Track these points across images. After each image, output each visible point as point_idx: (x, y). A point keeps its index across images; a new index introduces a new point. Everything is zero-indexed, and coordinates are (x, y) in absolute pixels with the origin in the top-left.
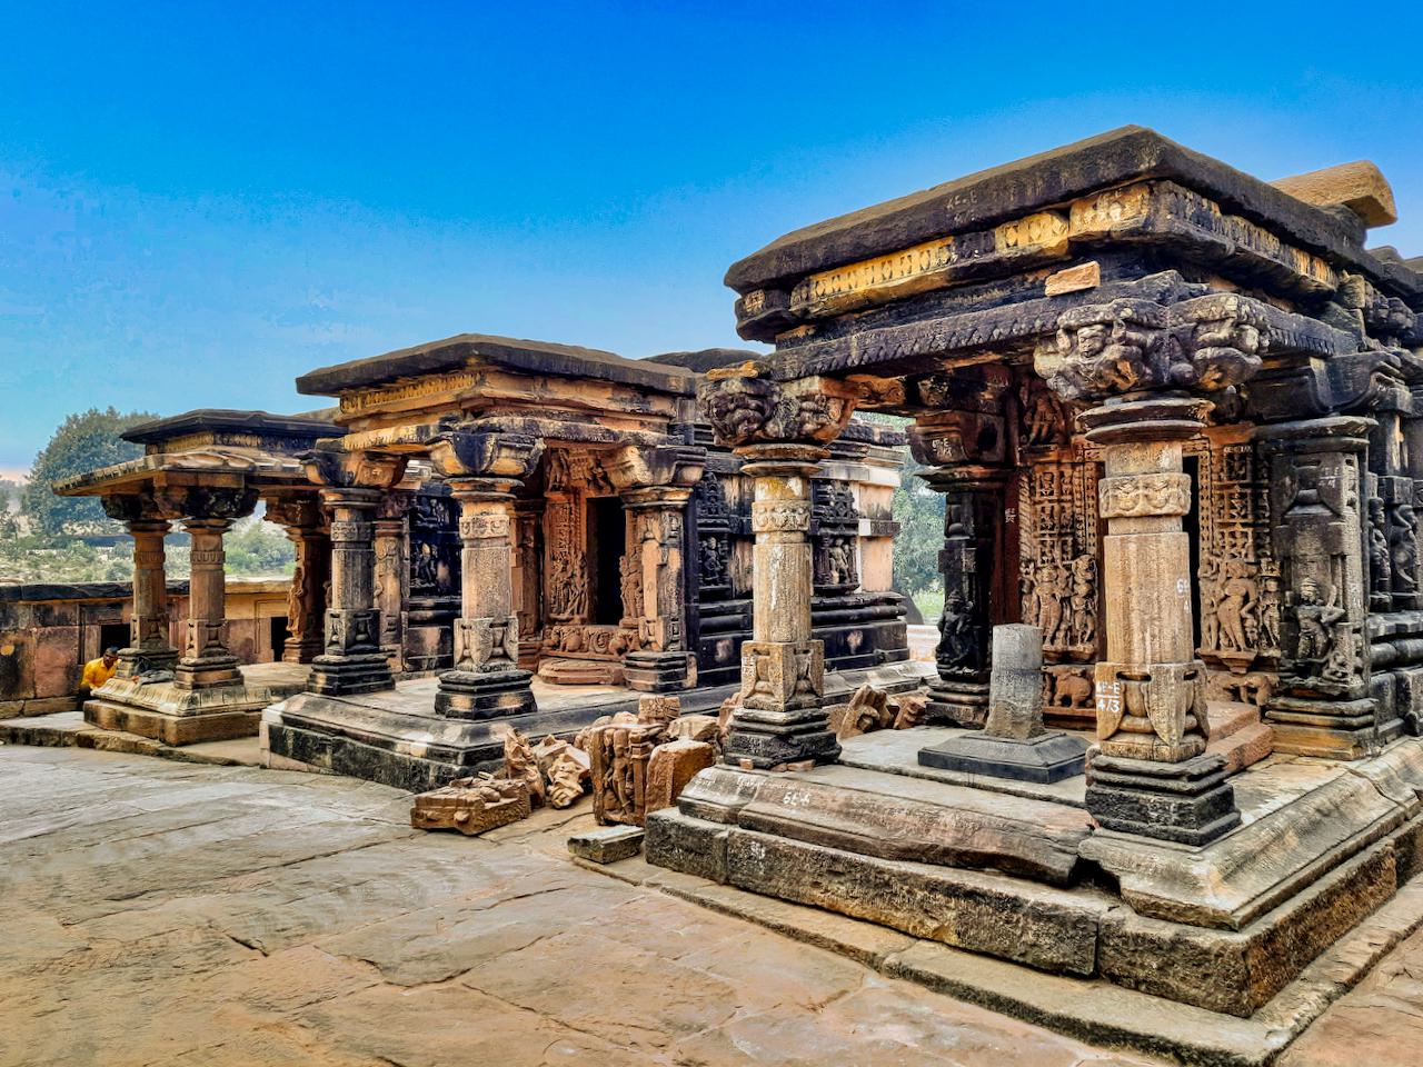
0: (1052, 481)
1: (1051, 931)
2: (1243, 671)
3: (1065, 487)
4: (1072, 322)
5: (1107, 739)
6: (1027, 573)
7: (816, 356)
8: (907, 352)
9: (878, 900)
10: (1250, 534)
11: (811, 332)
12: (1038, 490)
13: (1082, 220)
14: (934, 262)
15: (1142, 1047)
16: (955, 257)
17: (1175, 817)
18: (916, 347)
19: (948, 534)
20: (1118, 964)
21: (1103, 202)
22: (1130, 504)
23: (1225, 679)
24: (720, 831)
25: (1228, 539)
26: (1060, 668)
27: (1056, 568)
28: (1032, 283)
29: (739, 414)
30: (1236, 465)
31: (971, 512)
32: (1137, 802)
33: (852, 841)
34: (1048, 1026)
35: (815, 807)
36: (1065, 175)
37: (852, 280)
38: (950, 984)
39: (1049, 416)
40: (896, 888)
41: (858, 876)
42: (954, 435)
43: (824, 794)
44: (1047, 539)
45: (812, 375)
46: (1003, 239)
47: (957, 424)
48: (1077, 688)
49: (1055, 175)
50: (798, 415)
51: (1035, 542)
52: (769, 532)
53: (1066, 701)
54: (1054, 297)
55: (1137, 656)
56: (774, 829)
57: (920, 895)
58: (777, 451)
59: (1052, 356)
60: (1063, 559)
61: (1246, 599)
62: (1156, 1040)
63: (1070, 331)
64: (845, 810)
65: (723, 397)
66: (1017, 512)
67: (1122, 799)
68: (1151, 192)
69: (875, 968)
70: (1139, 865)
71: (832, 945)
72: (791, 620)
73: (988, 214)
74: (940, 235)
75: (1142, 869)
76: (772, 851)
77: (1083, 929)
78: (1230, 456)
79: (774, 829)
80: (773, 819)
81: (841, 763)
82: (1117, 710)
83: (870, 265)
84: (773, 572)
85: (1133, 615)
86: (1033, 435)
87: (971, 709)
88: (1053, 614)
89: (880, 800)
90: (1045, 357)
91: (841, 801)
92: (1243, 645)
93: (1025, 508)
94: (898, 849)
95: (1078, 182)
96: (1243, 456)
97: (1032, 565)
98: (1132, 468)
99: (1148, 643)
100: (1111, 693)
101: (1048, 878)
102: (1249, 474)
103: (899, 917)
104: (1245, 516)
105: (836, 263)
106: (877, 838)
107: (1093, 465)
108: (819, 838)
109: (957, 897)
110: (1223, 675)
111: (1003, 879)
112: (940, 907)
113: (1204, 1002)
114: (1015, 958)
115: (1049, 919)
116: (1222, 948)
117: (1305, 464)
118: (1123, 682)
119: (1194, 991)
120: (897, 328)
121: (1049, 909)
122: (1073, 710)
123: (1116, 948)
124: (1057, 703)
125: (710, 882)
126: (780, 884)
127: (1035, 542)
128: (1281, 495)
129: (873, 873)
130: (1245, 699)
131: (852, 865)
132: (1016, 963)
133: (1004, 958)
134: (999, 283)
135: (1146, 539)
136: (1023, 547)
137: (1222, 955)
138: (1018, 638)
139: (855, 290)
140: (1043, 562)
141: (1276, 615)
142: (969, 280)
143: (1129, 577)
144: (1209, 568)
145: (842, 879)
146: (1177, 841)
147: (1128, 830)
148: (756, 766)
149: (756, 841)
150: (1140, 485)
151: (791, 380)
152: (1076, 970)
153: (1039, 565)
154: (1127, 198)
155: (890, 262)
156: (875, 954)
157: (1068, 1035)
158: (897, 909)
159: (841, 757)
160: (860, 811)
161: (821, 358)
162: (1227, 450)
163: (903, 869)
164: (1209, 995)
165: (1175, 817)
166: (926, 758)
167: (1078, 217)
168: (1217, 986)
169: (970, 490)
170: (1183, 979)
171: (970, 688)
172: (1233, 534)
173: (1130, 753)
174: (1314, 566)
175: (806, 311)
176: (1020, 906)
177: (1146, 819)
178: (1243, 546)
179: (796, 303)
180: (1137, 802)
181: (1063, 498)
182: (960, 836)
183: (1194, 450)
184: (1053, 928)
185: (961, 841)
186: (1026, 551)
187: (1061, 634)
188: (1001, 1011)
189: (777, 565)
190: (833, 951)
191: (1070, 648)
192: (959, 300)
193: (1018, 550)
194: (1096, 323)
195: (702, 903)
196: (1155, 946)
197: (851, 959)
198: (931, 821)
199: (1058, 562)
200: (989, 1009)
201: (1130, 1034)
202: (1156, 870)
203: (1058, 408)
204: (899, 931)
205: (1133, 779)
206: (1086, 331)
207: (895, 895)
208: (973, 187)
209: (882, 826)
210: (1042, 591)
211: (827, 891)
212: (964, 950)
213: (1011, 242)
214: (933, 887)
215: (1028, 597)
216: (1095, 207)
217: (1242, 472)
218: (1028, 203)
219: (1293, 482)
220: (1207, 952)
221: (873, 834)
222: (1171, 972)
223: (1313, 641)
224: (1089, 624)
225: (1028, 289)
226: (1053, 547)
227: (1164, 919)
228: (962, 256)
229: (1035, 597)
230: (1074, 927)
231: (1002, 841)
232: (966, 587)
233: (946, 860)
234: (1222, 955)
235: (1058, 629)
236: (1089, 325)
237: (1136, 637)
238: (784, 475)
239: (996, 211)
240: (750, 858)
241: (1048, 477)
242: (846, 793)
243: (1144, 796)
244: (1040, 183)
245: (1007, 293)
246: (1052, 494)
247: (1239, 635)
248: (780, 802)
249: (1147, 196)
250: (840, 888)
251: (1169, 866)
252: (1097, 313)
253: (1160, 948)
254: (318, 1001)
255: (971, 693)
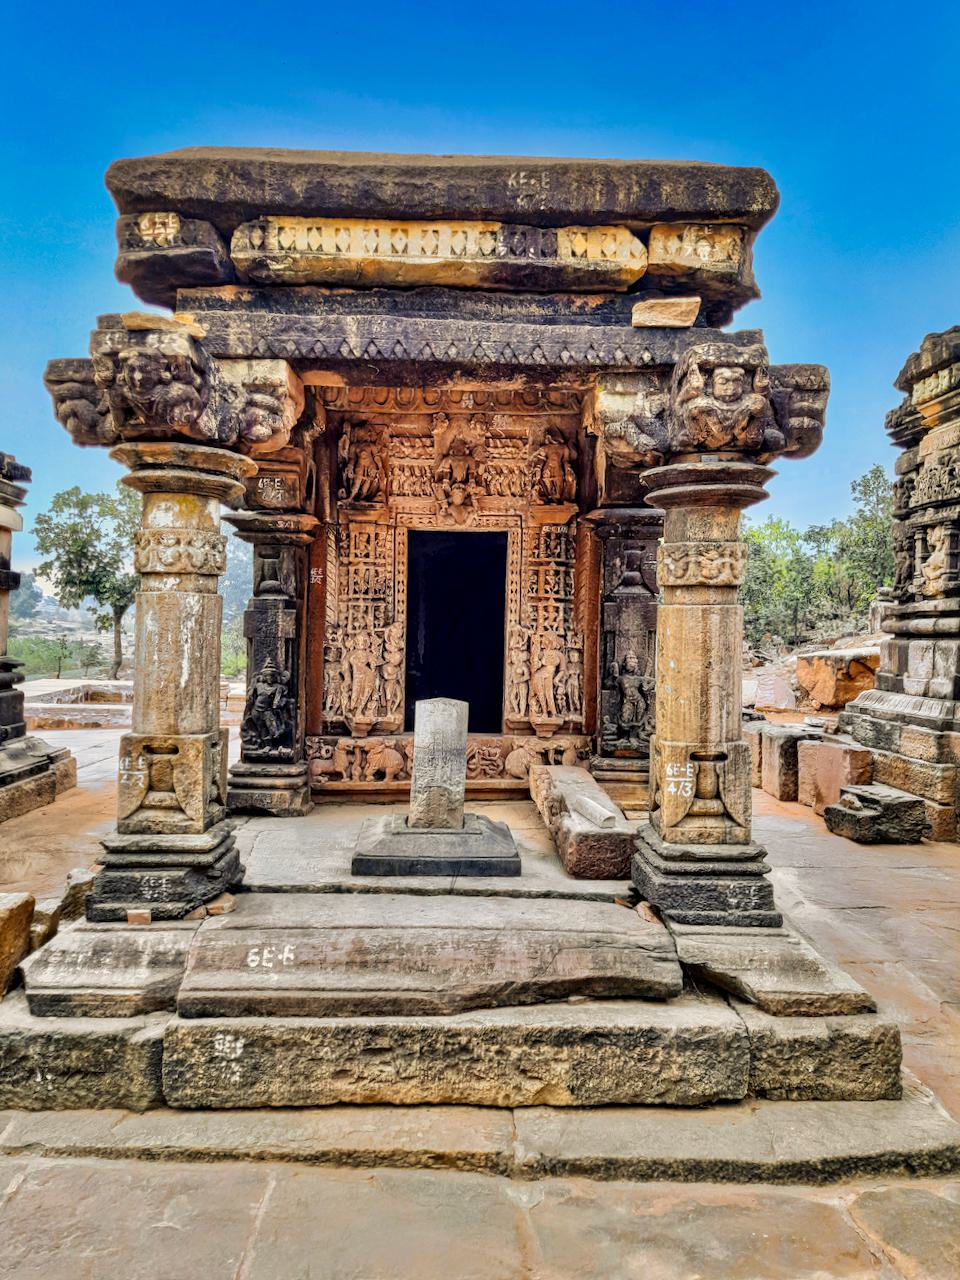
0: (368, 541)
1: (701, 1059)
2: (550, 735)
4: (712, 359)
5: (675, 826)
6: (333, 640)
7: (284, 331)
8: (439, 355)
9: (450, 1075)
10: (561, 609)
11: (246, 297)
12: (353, 550)
13: (666, 249)
14: (472, 248)
15: (874, 1169)
16: (502, 250)
17: (755, 900)
18: (453, 352)
19: (257, 593)
20: (771, 1077)
21: (690, 235)
22: (715, 572)
23: (535, 744)
24: (136, 1030)
25: (542, 613)
26: (373, 740)
28: (581, 307)
29: (177, 389)
30: (553, 544)
32: (715, 890)
33: (395, 1002)
34: (768, 1179)
35: (306, 964)
36: (666, 189)
37: (343, 239)
38: (627, 1164)
39: (373, 472)
40: (478, 1051)
41: (417, 1047)
42: (293, 476)
43: (313, 941)
45: (274, 357)
46: (568, 245)
48: (392, 761)
49: (654, 186)
50: (244, 411)
52: (179, 574)
53: (380, 775)
54: (640, 328)
55: (713, 735)
56: (250, 1008)
57: (515, 1052)
58: (207, 457)
59: (617, 397)
61: (558, 669)
62: (887, 1157)
63: (707, 370)
64: (358, 959)
65: (154, 358)
66: (324, 573)
67: (699, 889)
68: (742, 240)
69: (502, 1173)
70: (751, 960)
71: (424, 1158)
72: (207, 702)
73: (564, 207)
74: (486, 216)
75: (755, 964)
76: (257, 1043)
77: (737, 1049)
78: (548, 535)
79: (250, 1008)
80: (242, 994)
81: (248, 889)
82: (689, 793)
83: (372, 226)
84: (185, 634)
85: (712, 691)
86: (355, 491)
87: (287, 794)
89: (407, 937)
90: (610, 397)
91: (349, 947)
92: (554, 712)
93: (332, 568)
94: (464, 998)
95: (682, 202)
96: (558, 536)
98: (716, 534)
99: (724, 720)
100: (684, 774)
101: (651, 994)
102: (563, 554)
103: (483, 1089)
104: (557, 592)
105: (320, 208)
106: (431, 991)
107: (405, 530)
108: (334, 1008)
109: (572, 1044)
110: (534, 739)
111: (594, 1006)
112: (546, 1062)
113: (862, 1094)
114: (649, 1100)
115: (698, 1045)
116: (883, 1034)
117: (632, 548)
118: (696, 763)
119: (851, 1086)
120: (422, 323)
121: (697, 1034)
122: (388, 783)
123: (771, 1062)
125: (119, 1113)
126: (273, 1088)
127: (343, 606)
128: (611, 574)
129: (442, 1039)
130: (552, 762)
131: (404, 1035)
132: (652, 1106)
133: (635, 1104)
134: (537, 297)
135: (727, 610)
136: (329, 612)
137: (883, 1042)
138: (455, 715)
139: (344, 255)
140: (354, 628)
141: (576, 683)
142: (510, 284)
143: (708, 651)
145: (388, 1057)
146: (760, 926)
147: (708, 921)
148: (157, 917)
149: (226, 1032)
150: (728, 552)
151: (236, 358)
152: (730, 1096)
153: (350, 630)
154: (717, 238)
155: (405, 231)
156: (498, 1154)
157: (793, 1183)
158: (479, 1078)
159: (246, 881)
160: (383, 957)
161: (294, 335)
162: (546, 529)
163: (489, 1025)
164: (867, 1084)
165: (755, 900)
166: (362, 866)
167: (661, 244)
168: (876, 1075)
169: (292, 543)
170: (840, 1076)
171: (286, 769)
172: (546, 609)
173: (701, 838)
175: (260, 264)
176: (658, 1037)
177: (725, 906)
178: (555, 620)
179: (243, 247)
180: (715, 890)
182: (537, 964)
183: (506, 525)
184: (701, 1055)
185: (540, 970)
186: (331, 616)
187: (373, 705)
188: (704, 1180)
189: (191, 624)
190: (427, 1166)
191: (380, 719)
192: (482, 306)
193: (323, 615)
194: (737, 365)
195: (149, 1155)
196: (811, 1047)
197: (460, 1169)
198: (491, 953)
200: (686, 1180)
201: (861, 1159)
202: (771, 963)
204: (490, 1107)
205: (710, 866)
206: (727, 373)
207: (478, 1060)
208: (547, 169)
209: (423, 969)
210: (358, 659)
211: (361, 1078)
212: (583, 1107)
213: (577, 249)
214: (534, 1039)
216: (680, 238)
217: (558, 551)
218: (618, 209)
219: (622, 564)
220: (866, 1042)
221: (427, 986)
222: (828, 1071)
223: (635, 706)
225: (575, 314)
226: (366, 612)
227: (807, 1015)
228: (512, 251)
230: (728, 1047)
231: (594, 960)
232: (281, 657)
233: (522, 998)
234: (883, 1042)
235: (370, 698)
236: (729, 366)
237: (714, 714)
238: (202, 492)
239: (574, 206)
240: (211, 1060)
242: (351, 935)
243: (721, 882)
244: (636, 189)
245: (549, 311)
246: (367, 556)
247: (552, 703)
248: (243, 965)
249: (738, 241)
250: (379, 1073)
251: (782, 955)
252: (741, 354)
253: (817, 1049)
255: (289, 776)
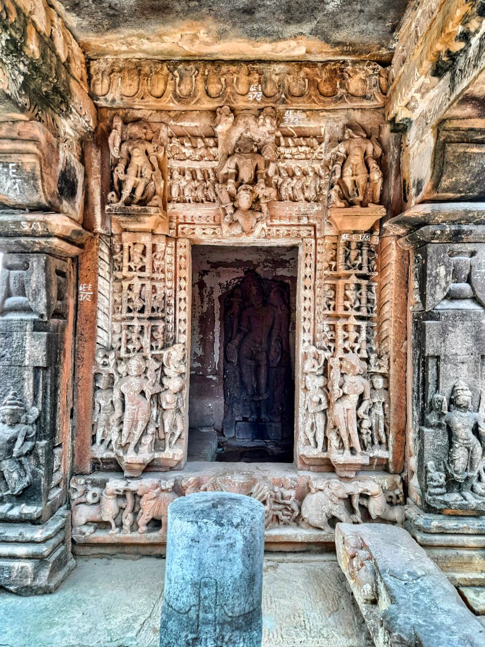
0: (144, 253)
3: (157, 263)
6: (105, 365)
12: (126, 263)
27: (145, 358)
31: (42, 279)
44: (135, 323)
47: (34, 140)
51: (116, 327)
60: (152, 348)
78: (348, 244)
86: (126, 193)
87: (29, 565)
88: (140, 416)
93: (104, 286)
97: (112, 355)
104: (358, 309)
124: (143, 528)
127: (116, 327)
136: (100, 332)
140: (128, 351)
144: (315, 362)
153: (123, 354)
174: (465, 367)
178: (356, 341)
181: (155, 276)
186: (103, 338)
187: (148, 440)
191: (157, 455)
199: (148, 352)
203: (156, 165)
215: (104, 394)
217: (358, 262)
224: (179, 424)
226: (141, 333)
229: (116, 396)
235: (144, 433)
241: (139, 249)
254: (321, 52)
255: (32, 542)
